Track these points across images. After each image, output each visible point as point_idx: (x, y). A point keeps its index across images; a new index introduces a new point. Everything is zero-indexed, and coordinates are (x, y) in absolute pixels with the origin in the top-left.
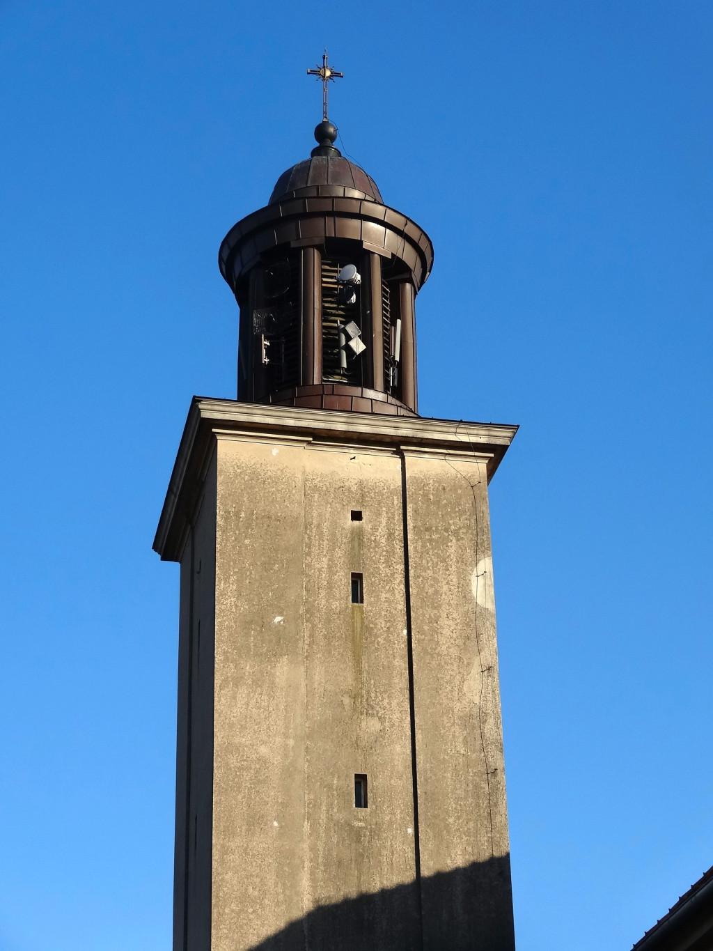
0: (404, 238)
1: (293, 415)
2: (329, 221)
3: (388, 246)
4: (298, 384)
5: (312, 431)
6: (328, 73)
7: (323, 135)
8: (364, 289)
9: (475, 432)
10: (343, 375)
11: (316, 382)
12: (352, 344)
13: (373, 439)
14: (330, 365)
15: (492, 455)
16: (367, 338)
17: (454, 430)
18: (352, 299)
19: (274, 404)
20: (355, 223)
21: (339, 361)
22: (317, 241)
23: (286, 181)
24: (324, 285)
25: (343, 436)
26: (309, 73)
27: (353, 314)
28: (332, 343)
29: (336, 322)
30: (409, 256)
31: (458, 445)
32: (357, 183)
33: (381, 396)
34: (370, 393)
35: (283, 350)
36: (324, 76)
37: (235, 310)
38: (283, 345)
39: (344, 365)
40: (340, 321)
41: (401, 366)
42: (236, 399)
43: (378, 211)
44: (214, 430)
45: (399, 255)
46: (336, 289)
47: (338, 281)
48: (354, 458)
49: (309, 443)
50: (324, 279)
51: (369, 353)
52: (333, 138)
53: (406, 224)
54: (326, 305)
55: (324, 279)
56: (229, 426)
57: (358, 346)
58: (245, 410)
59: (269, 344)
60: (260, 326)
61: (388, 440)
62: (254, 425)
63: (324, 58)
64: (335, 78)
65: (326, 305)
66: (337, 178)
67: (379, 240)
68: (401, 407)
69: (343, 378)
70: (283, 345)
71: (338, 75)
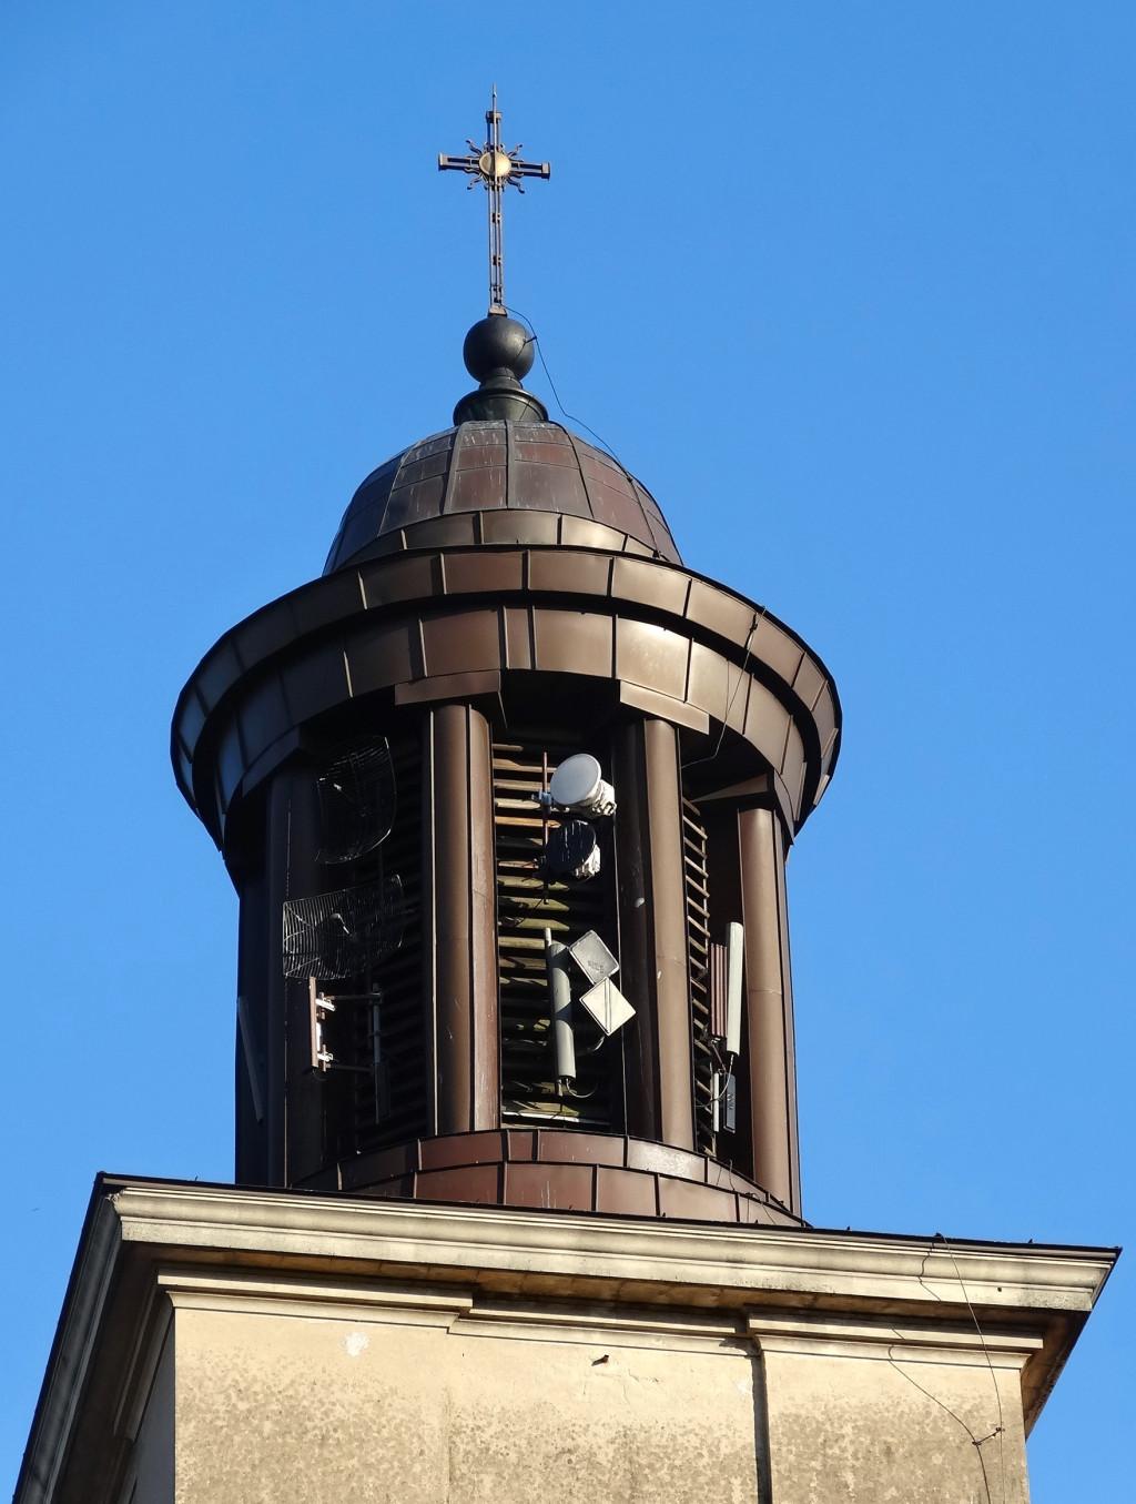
0: (749, 670)
1: (410, 1228)
2: (514, 619)
4: (425, 1132)
5: (471, 1276)
6: (503, 167)
7: (487, 353)
8: (626, 833)
9: (983, 1271)
10: (567, 1101)
12: (593, 1001)
13: (662, 1299)
14: (525, 1070)
15: (1037, 1343)
16: (637, 981)
17: (915, 1266)
18: (589, 861)
21: (552, 1055)
23: (374, 496)
24: (500, 820)
26: (443, 168)
30: (766, 727)
32: (598, 500)
33: (685, 1165)
34: (648, 1155)
39: (569, 1067)
40: (553, 932)
41: (744, 1068)
42: (232, 1181)
43: (665, 588)
44: (163, 1280)
46: (538, 832)
48: (604, 1360)
49: (462, 1314)
50: (502, 803)
51: (642, 1030)
52: (520, 367)
53: (754, 627)
54: (510, 881)
55: (502, 803)
57: (610, 1009)
58: (260, 1216)
59: (331, 1007)
61: (709, 1301)
62: (288, 1262)
63: (490, 119)
64: (525, 181)
65: (510, 881)
66: (535, 486)
67: (669, 680)
68: (748, 1196)
69: (565, 1109)
71: (535, 171)
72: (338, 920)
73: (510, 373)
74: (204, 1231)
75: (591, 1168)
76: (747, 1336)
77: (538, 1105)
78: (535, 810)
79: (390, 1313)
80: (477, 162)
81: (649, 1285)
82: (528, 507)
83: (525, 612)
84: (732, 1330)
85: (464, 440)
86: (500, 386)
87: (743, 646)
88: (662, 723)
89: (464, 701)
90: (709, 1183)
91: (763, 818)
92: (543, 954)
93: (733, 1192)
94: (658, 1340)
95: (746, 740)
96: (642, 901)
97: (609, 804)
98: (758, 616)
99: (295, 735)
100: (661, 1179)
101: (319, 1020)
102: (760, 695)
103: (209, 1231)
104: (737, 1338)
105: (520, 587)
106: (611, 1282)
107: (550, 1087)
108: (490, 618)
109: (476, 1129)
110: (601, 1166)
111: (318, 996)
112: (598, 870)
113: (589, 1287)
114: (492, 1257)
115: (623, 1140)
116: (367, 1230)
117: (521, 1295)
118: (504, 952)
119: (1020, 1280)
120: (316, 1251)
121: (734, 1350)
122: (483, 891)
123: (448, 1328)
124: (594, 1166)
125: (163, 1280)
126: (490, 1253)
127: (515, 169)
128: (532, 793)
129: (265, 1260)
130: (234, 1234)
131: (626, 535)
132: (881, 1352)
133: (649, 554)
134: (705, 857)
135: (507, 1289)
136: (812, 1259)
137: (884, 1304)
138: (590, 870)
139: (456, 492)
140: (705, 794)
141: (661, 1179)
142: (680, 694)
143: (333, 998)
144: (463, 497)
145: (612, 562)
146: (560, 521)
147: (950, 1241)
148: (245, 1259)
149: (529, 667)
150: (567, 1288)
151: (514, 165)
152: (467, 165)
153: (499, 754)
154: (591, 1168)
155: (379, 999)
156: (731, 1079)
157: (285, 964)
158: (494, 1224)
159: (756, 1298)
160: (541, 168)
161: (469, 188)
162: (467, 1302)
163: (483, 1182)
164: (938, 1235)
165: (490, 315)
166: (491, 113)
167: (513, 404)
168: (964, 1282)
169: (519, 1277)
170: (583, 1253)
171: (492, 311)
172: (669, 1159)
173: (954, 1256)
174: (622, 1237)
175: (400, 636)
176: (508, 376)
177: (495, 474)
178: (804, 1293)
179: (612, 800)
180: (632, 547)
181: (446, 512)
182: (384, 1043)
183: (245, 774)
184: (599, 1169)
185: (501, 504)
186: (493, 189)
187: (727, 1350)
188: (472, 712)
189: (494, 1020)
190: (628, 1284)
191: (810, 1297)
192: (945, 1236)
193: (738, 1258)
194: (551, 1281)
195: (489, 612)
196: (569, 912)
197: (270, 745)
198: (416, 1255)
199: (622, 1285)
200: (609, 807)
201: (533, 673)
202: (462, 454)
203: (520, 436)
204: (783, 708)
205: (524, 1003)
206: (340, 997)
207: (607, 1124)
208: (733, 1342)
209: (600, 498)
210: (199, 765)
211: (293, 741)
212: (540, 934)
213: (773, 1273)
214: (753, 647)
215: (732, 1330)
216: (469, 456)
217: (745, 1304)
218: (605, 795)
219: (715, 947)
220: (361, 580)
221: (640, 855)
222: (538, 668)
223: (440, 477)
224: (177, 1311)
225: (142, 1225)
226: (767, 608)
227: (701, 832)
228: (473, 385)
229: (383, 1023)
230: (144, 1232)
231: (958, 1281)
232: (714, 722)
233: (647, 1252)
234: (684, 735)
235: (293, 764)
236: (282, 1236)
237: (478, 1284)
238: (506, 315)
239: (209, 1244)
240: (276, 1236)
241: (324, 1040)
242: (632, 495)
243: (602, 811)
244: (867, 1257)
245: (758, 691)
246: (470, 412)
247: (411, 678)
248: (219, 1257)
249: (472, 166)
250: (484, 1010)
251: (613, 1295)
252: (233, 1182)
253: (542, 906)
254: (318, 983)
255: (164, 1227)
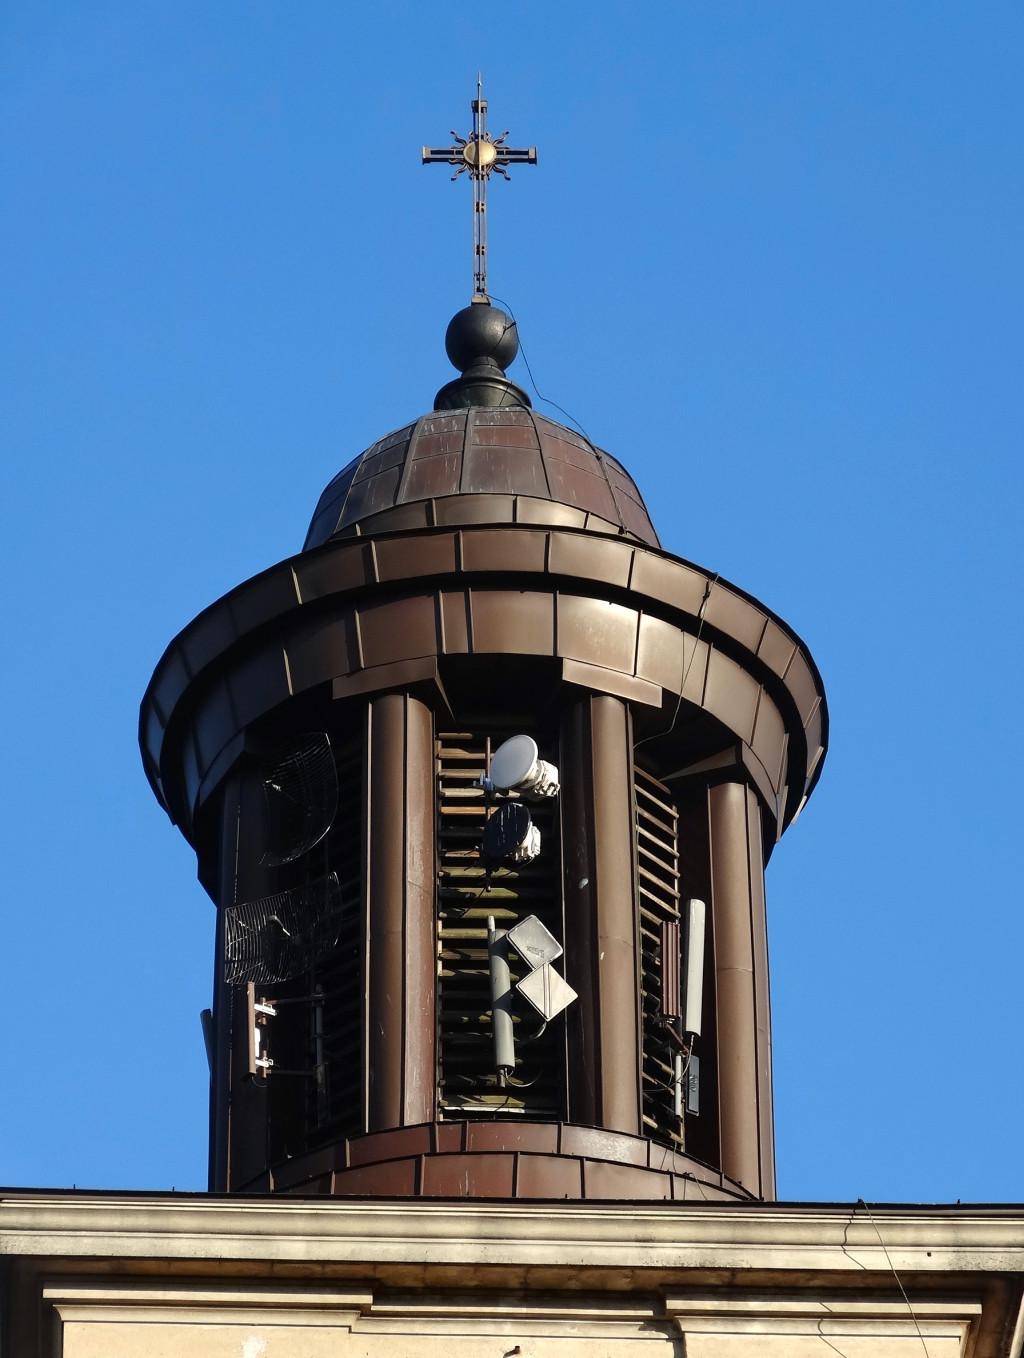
0: (704, 638)
1: (301, 1225)
2: (449, 604)
3: (651, 669)
4: (357, 1133)
5: (368, 1272)
6: (488, 155)
7: (471, 346)
8: (570, 816)
9: (910, 1235)
10: (510, 1091)
11: (413, 1115)
12: (529, 987)
13: (573, 1285)
14: (463, 1062)
15: (975, 1309)
16: (580, 966)
17: (836, 1235)
18: (527, 842)
19: (282, 1194)
20: (534, 605)
21: (491, 1047)
22: (414, 672)
23: (336, 494)
24: (446, 810)
25: (473, 1283)
27: (560, 894)
28: (465, 998)
29: (482, 923)
30: (726, 694)
31: (859, 1283)
32: (558, 479)
33: (625, 1149)
34: (589, 1141)
35: (319, 1030)
37: (214, 909)
38: (319, 1011)
39: (508, 1056)
40: (496, 920)
41: (709, 1047)
42: (205, 1189)
43: (612, 561)
44: (48, 1293)
45: (692, 694)
46: (481, 819)
47: (489, 793)
48: (516, 1351)
49: (363, 1312)
50: (450, 792)
51: (584, 1016)
52: (504, 355)
53: (706, 596)
54: (456, 872)
55: (450, 792)
56: (90, 1275)
57: (551, 994)
58: (143, 1221)
59: (272, 1012)
60: (248, 958)
61: (623, 1284)
62: (175, 1268)
63: (475, 109)
64: (511, 169)
65: (456, 872)
66: (491, 468)
67: (623, 655)
68: (686, 1176)
69: (511, 1101)
70: (319, 1011)
71: (522, 157)
72: (274, 922)
73: (492, 361)
74: (85, 1240)
75: (512, 1156)
76: (665, 1318)
77: (484, 1098)
78: (477, 798)
79: (321, 1316)
80: (461, 153)
81: (556, 1271)
82: (481, 491)
83: (462, 594)
84: (650, 1313)
86: (478, 374)
87: (697, 615)
88: (610, 699)
89: (404, 690)
90: (651, 1166)
91: (735, 792)
92: (481, 944)
93: (668, 1173)
94: (573, 1328)
95: (706, 711)
96: (585, 882)
97: (552, 784)
98: (711, 583)
99: (242, 737)
100: (587, 1164)
101: (258, 1025)
102: (721, 662)
103: (90, 1240)
104: (658, 1321)
105: (453, 569)
106: (517, 1270)
107: (493, 1079)
108: (427, 603)
109: (406, 1124)
110: (523, 1153)
111: (258, 1001)
112: (537, 852)
113: (494, 1276)
114: (387, 1250)
115: (556, 1126)
116: (255, 1229)
117: (423, 1288)
118: (449, 943)
119: (951, 1243)
120: (202, 1255)
121: (654, 1334)
122: (420, 882)
123: (350, 1327)
124: (515, 1154)
125: (49, 1293)
126: (385, 1247)
127: (501, 157)
128: (474, 779)
129: (153, 1267)
130: (117, 1241)
131: (587, 512)
132: (908, 1329)
133: (614, 531)
134: (676, 837)
135: (410, 1283)
136: (726, 1233)
137: (808, 1276)
138: (529, 853)
139: (411, 482)
140: (673, 772)
141: (587, 1164)
142: (628, 667)
143: (274, 1002)
144: (417, 485)
145: (548, 537)
146: (515, 502)
147: (871, 1206)
148: (132, 1267)
149: (467, 651)
150: (471, 1279)
151: (499, 153)
153: (447, 744)
154: (512, 1156)
155: (320, 1001)
156: (694, 1063)
157: (226, 971)
158: (389, 1217)
159: (672, 1278)
160: (527, 153)
162: (366, 1299)
163: (399, 1173)
164: (860, 1201)
165: (473, 304)
166: (477, 102)
168: (887, 1248)
169: (418, 1270)
170: (638, 1244)
171: (474, 301)
172: (614, 1145)
173: (875, 1222)
174: (524, 1222)
175: (338, 628)
176: (490, 367)
177: (451, 460)
178: (719, 1269)
179: (556, 781)
180: (595, 524)
181: (398, 503)
182: (326, 1047)
183: (202, 783)
184: (520, 1157)
185: (454, 490)
186: (478, 178)
187: (647, 1334)
188: (411, 702)
189: (429, 1012)
190: (534, 1270)
191: (727, 1274)
192: (866, 1201)
193: (647, 1237)
194: (452, 1272)
195: (425, 597)
196: (518, 898)
197: (221, 751)
198: (308, 1252)
199: (528, 1272)
200: (553, 788)
201: (471, 656)
202: (420, 443)
203: (480, 421)
204: (750, 676)
205: (465, 998)
206: (282, 1001)
207: (554, 1113)
208: (652, 1325)
209: (561, 478)
210: (166, 775)
211: (240, 745)
212: (482, 923)
213: (687, 1250)
214: (707, 614)
215: (650, 1313)
216: (427, 445)
217: (662, 1285)
218: (548, 776)
219: (667, 925)
220: (295, 575)
221: (585, 834)
222: (476, 650)
223: (397, 468)
224: (66, 1325)
225: (21, 1238)
226: (720, 575)
227: (673, 812)
228: (457, 374)
229: (325, 1025)
230: (22, 1245)
231: (881, 1248)
232: (667, 695)
233: (552, 1236)
234: (633, 708)
235: (244, 769)
236: (167, 1241)
237: (378, 1280)
238: (489, 304)
239: (90, 1253)
240: (161, 1241)
241: (262, 1046)
242: (598, 473)
243: (545, 792)
244: (54, 1215)
245: (717, 657)
247: (348, 671)
248: (104, 1267)
249: (456, 156)
250: (418, 1002)
251: (521, 1283)
252: (206, 1190)
253: (485, 894)
254: (257, 989)
255: (43, 1239)
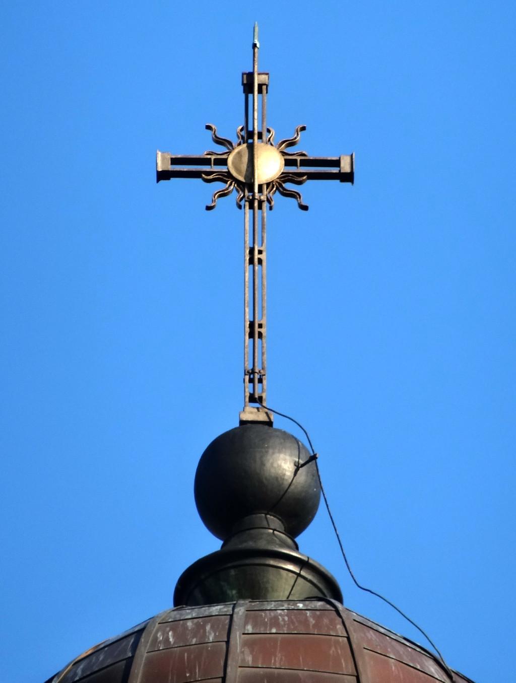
6: (269, 165)
7: (242, 497)
26: (163, 176)
36: (247, 185)
52: (297, 512)
63: (248, 87)
64: (309, 190)
71: (328, 170)
73: (274, 522)
80: (224, 162)
85: (156, 638)
151: (288, 163)
152: (206, 168)
160: (337, 163)
161: (209, 208)
165: (242, 423)
166: (250, 76)
167: (271, 574)
176: (270, 531)
186: (252, 207)
202: (150, 662)
228: (212, 544)
238: (269, 423)
246: (197, 594)
